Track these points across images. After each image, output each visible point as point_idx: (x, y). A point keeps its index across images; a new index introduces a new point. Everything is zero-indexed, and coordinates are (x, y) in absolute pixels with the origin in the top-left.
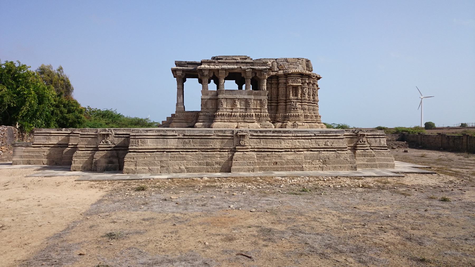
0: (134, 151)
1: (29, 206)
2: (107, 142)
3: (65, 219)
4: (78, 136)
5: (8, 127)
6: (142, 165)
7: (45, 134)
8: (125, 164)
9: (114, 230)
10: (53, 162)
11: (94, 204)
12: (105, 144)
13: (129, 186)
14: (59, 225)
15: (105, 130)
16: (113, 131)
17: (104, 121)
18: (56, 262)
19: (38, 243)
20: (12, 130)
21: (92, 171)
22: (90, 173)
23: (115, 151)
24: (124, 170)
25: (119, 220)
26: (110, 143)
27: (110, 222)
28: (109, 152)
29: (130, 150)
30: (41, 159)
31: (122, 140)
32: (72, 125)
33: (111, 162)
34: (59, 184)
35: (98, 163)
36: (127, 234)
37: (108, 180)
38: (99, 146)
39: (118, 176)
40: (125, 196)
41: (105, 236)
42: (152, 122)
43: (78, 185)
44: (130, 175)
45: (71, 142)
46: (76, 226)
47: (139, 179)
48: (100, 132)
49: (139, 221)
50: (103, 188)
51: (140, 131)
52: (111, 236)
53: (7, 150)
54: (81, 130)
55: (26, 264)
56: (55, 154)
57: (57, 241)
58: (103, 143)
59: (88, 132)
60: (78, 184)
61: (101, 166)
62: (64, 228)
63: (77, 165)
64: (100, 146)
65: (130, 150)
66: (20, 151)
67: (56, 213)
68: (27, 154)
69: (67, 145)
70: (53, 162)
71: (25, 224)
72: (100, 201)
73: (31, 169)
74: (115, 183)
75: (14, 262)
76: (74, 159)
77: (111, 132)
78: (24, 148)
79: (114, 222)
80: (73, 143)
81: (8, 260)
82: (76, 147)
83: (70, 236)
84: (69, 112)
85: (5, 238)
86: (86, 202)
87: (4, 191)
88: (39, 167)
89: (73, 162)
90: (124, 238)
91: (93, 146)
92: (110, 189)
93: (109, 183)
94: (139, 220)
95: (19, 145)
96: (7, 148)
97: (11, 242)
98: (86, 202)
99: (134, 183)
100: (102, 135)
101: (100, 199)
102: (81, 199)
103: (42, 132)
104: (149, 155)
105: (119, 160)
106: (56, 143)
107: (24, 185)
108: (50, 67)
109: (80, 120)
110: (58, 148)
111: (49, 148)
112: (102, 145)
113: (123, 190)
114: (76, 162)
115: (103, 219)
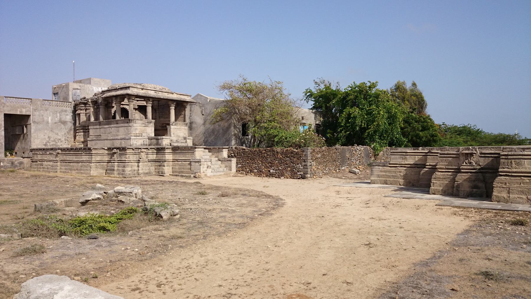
0: (506, 174)
1: (392, 227)
2: (471, 162)
3: (430, 247)
4: (437, 156)
5: (365, 146)
6: (518, 193)
7: (401, 154)
8: (495, 190)
9: (491, 269)
10: (410, 183)
11: (461, 234)
12: (469, 165)
13: (502, 218)
14: (424, 252)
15: (469, 149)
16: (477, 149)
17: (462, 140)
18: (426, 291)
19: (405, 268)
20: (368, 149)
21: (453, 196)
22: (451, 198)
23: (480, 174)
24: (494, 197)
25: (495, 258)
26: (474, 164)
27: (484, 259)
28: (474, 174)
29: (500, 173)
30: (398, 180)
31: (489, 161)
32: (426, 144)
33: (475, 187)
34: (419, 207)
35: (461, 187)
36: (509, 277)
37: (474, 208)
38: (461, 167)
39: (486, 204)
40: (497, 229)
41: (479, 275)
42: (523, 138)
43: (439, 211)
44: (501, 205)
45: (429, 163)
46: (443, 256)
47: (515, 211)
48: (463, 151)
49: (521, 263)
50: (468, 217)
51: (514, 150)
52: (487, 275)
53: (364, 169)
54: (440, 148)
55: (396, 287)
56: (411, 175)
57: (424, 270)
58: (466, 163)
59: (449, 151)
60: (440, 209)
61: (464, 190)
62: (428, 257)
63: (436, 188)
64: (463, 167)
65: (500, 173)
66: (377, 170)
67: (419, 238)
68: (384, 174)
69: (424, 166)
70: (410, 183)
71: (390, 245)
72: (467, 232)
73: (389, 189)
74: (483, 213)
75: (385, 282)
76: (433, 181)
77: (476, 151)
78: (381, 168)
79: (489, 259)
80: (431, 164)
81: (379, 279)
82: (434, 167)
83: (438, 267)
84: (424, 129)
85: (373, 256)
86: (451, 230)
87: (366, 209)
88: (395, 187)
89: (432, 184)
90: (505, 281)
91: (454, 167)
92: (478, 219)
93: (476, 212)
94: (522, 262)
95: (377, 164)
96: (364, 168)
97: (379, 261)
98: (451, 230)
99: (508, 215)
100: (464, 154)
101: (467, 229)
102: (444, 227)
103: (398, 151)
104: (528, 181)
105: (485, 185)
106: (412, 163)
107: (384, 205)
108: (404, 83)
109: (436, 139)
110: (415, 169)
111: (405, 168)
112: (465, 166)
113: (494, 222)
114: (435, 185)
115: (474, 253)
